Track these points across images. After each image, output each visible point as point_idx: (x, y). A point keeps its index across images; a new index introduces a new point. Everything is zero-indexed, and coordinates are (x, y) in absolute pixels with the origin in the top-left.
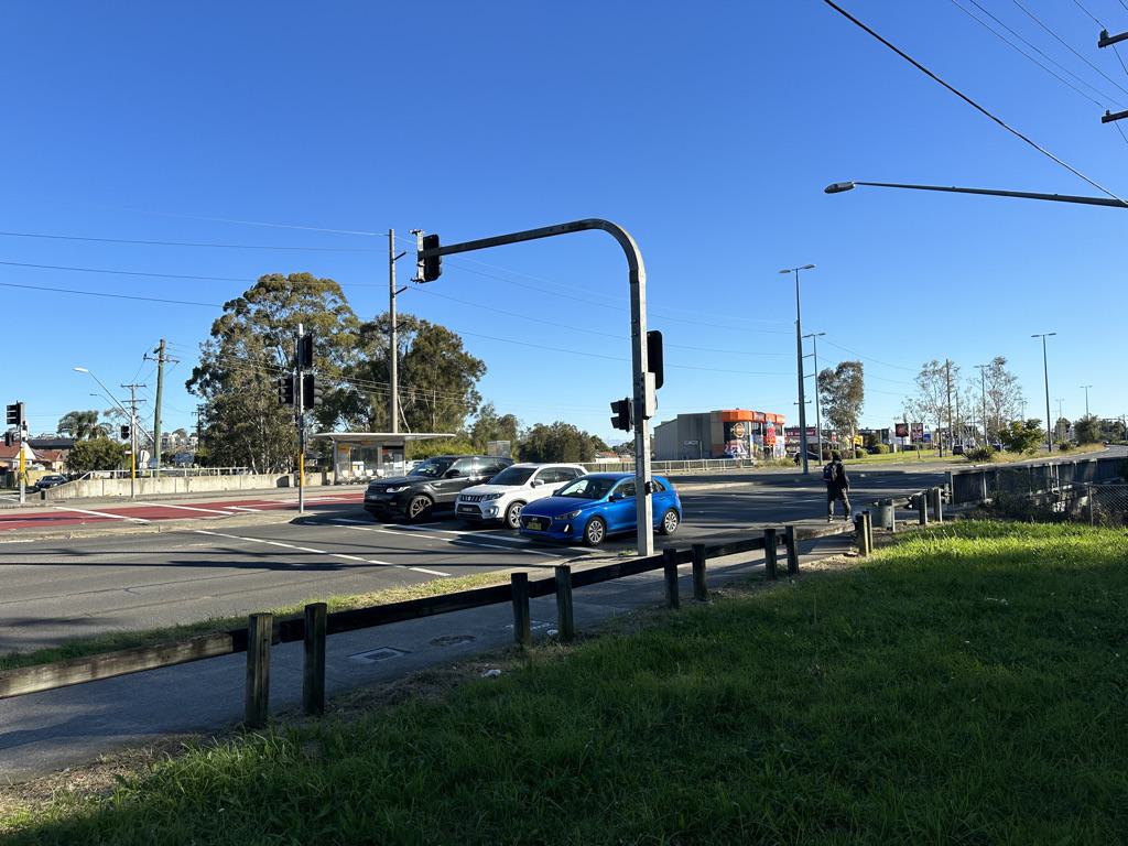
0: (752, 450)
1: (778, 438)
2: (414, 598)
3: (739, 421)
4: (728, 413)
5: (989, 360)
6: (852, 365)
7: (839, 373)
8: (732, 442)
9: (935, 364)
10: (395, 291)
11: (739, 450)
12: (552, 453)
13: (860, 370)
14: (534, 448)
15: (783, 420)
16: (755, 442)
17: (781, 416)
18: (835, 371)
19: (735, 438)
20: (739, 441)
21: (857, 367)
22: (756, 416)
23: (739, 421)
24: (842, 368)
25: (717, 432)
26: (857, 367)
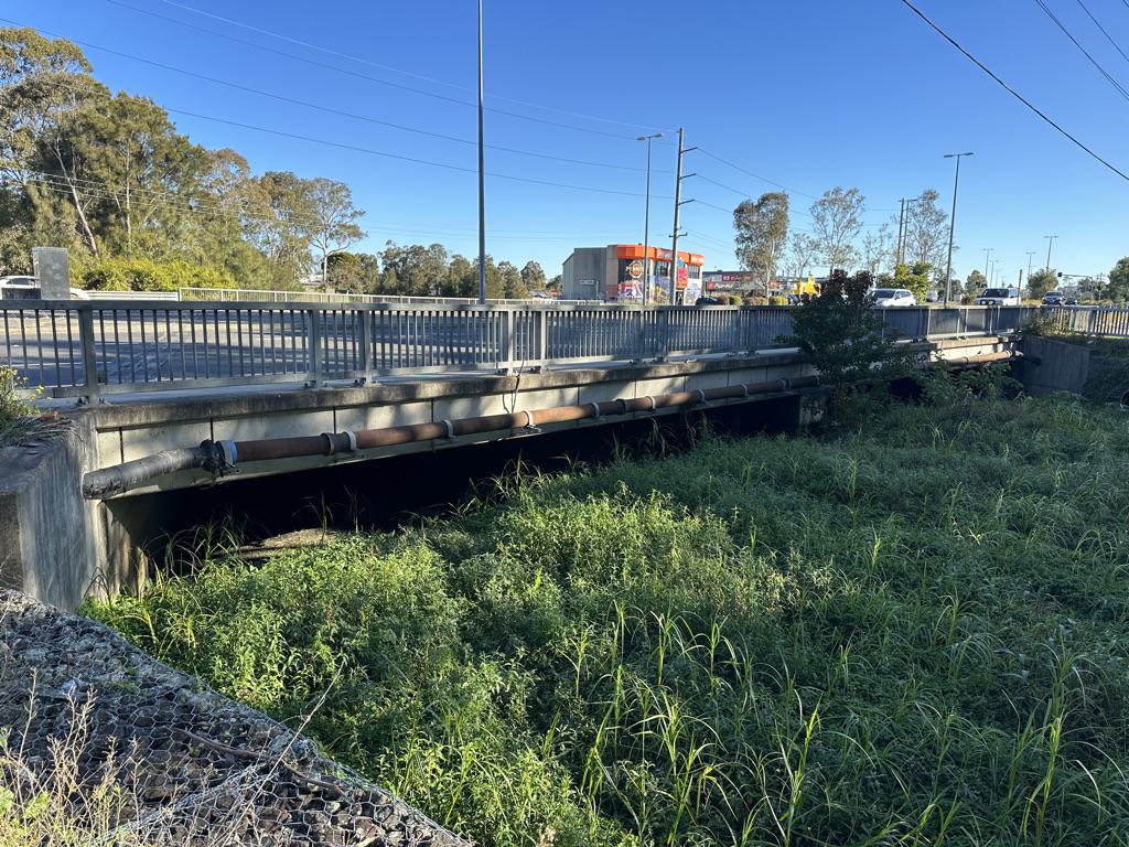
0: (652, 293)
1: (691, 282)
2: (321, 466)
3: (637, 258)
4: (623, 249)
5: (918, 193)
6: (775, 197)
7: (760, 205)
8: (627, 282)
9: (837, 191)
10: (680, 201)
11: (634, 293)
12: (470, 289)
13: (785, 204)
14: (450, 282)
15: (701, 260)
16: (657, 285)
17: (699, 256)
18: (756, 203)
19: (630, 278)
20: (634, 282)
21: (781, 199)
22: (659, 253)
23: (637, 258)
24: (765, 199)
25: (612, 269)
26: (781, 199)
